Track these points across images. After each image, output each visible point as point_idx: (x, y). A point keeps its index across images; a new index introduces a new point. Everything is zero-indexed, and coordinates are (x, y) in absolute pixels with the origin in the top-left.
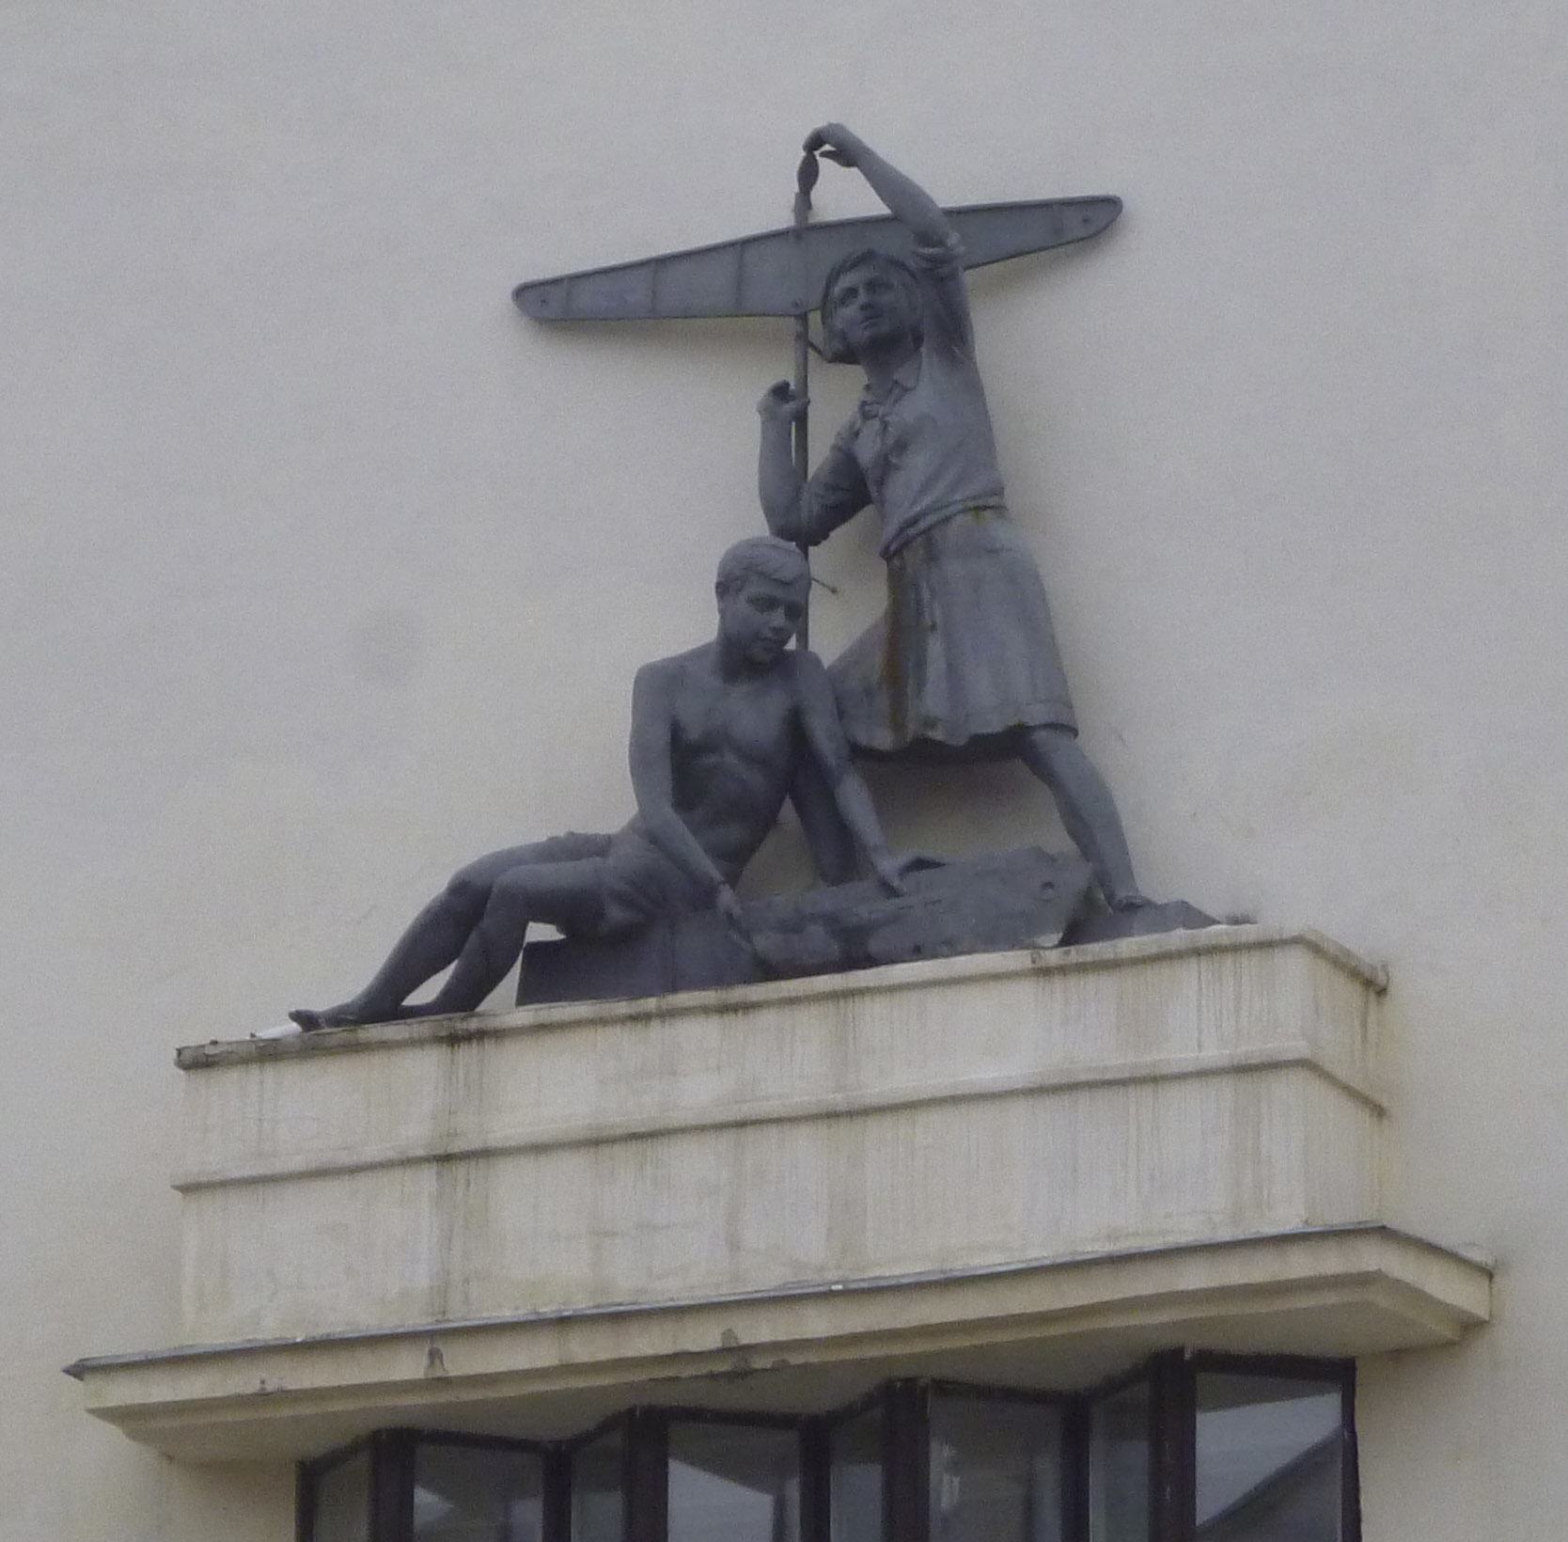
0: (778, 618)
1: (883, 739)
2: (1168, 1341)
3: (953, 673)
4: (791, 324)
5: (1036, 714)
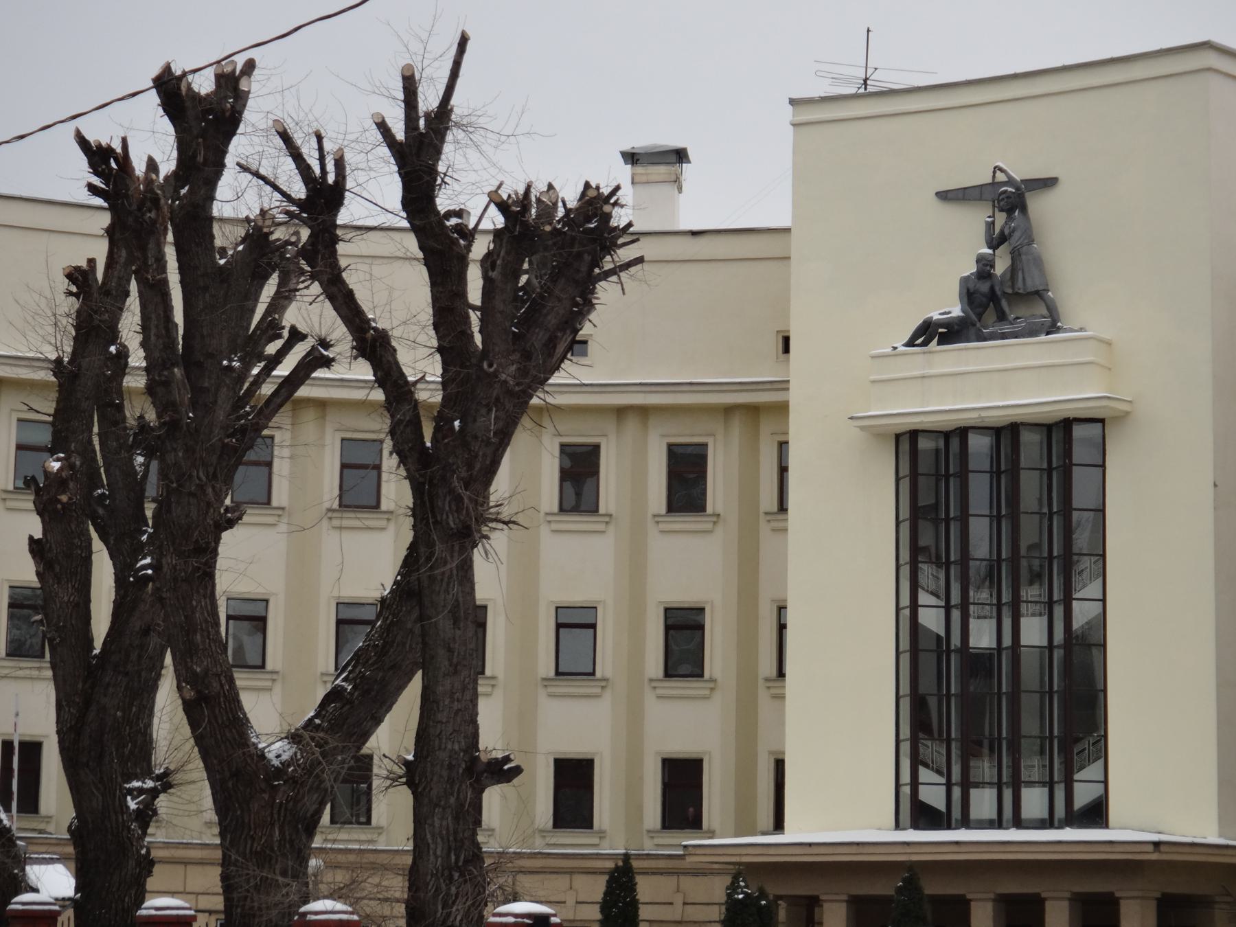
0: (988, 268)
1: (1010, 291)
2: (1014, 419)
3: (1024, 279)
4: (991, 203)
5: (1041, 288)
